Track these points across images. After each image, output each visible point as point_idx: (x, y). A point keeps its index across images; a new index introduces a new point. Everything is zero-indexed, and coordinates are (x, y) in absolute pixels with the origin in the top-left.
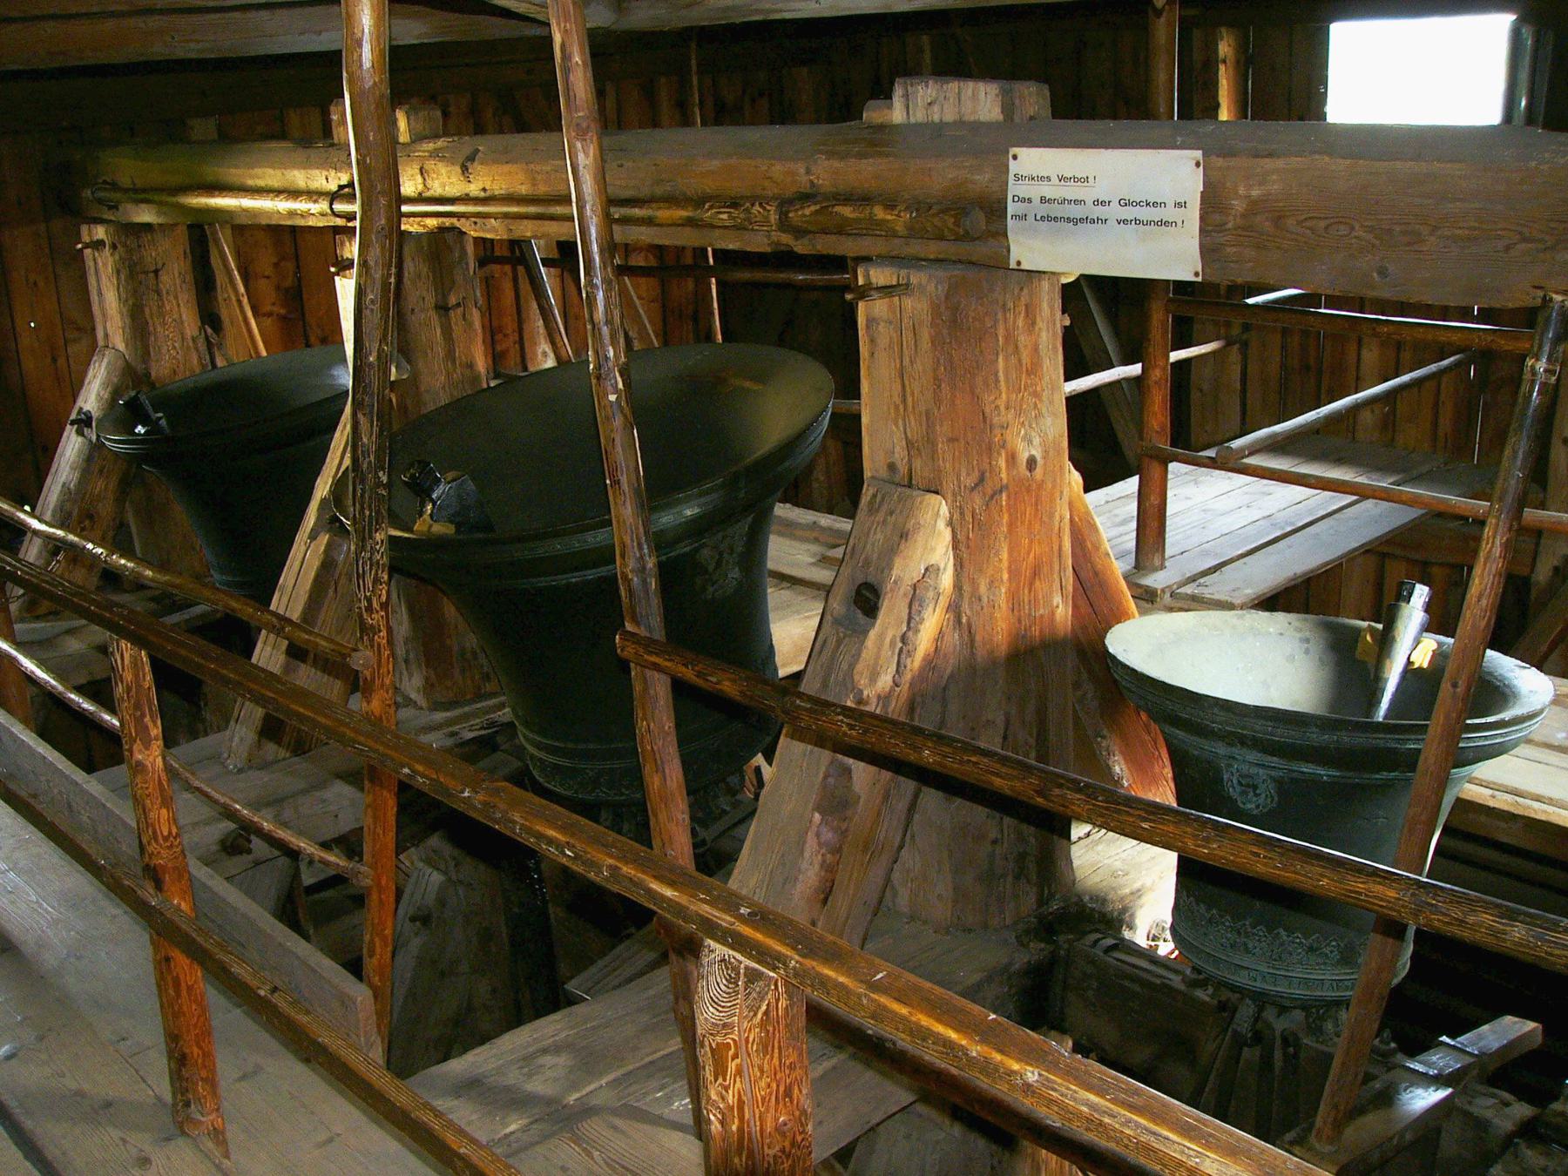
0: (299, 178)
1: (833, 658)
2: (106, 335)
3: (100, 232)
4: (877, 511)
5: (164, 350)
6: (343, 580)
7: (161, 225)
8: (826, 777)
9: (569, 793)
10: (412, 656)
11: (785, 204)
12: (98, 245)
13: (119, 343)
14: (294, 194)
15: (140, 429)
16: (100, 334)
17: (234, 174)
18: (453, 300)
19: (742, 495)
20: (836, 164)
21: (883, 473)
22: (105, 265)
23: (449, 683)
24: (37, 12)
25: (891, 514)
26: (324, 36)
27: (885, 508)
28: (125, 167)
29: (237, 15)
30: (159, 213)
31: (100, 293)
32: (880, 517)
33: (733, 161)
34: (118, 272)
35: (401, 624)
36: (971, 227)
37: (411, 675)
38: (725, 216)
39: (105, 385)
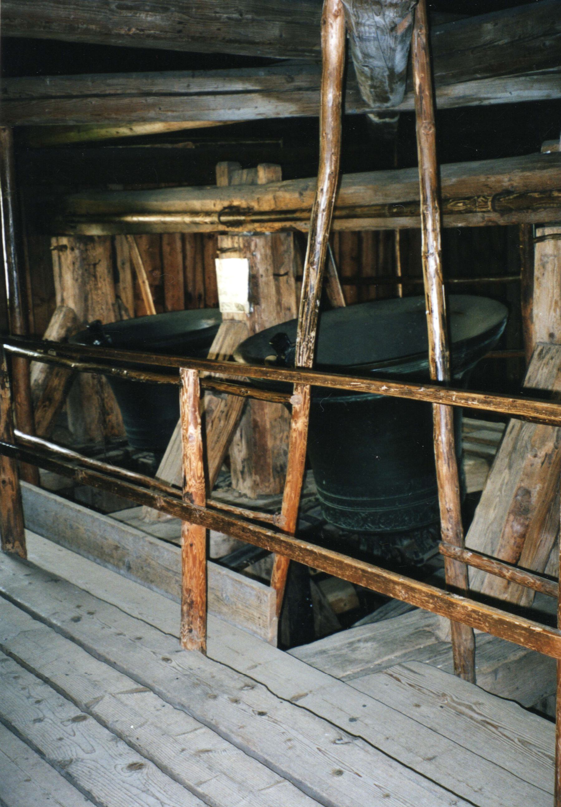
0: (197, 204)
1: (518, 435)
2: (63, 300)
3: (64, 241)
4: (543, 358)
5: (97, 309)
6: (216, 421)
7: (99, 237)
8: (516, 496)
9: (348, 528)
10: (246, 470)
11: (496, 197)
12: (62, 248)
13: (71, 304)
14: (195, 213)
15: (97, 342)
16: (58, 299)
17: (155, 203)
18: (282, 272)
19: (463, 356)
20: (528, 174)
21: (546, 339)
22: (66, 259)
23: (267, 484)
24: (89, 93)
25: (552, 358)
26: (242, 111)
27: (548, 356)
28: (84, 202)
29: (195, 98)
30: (103, 230)
31: (61, 276)
32: (545, 360)
33: (464, 177)
34: (74, 263)
35: (240, 451)
36: (274, 447)
37: (244, 480)
38: (461, 204)
39: (61, 326)
